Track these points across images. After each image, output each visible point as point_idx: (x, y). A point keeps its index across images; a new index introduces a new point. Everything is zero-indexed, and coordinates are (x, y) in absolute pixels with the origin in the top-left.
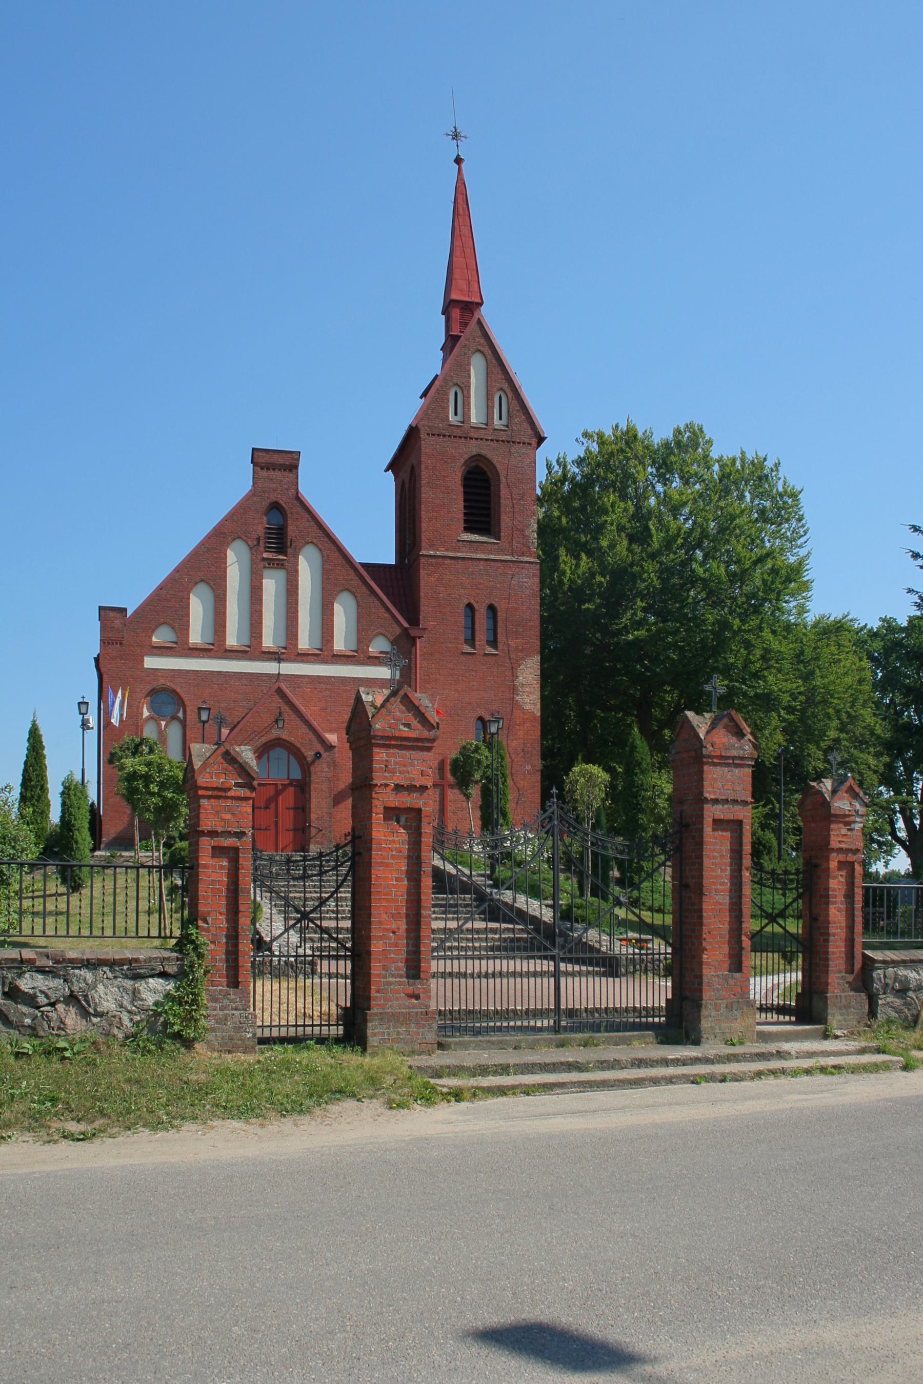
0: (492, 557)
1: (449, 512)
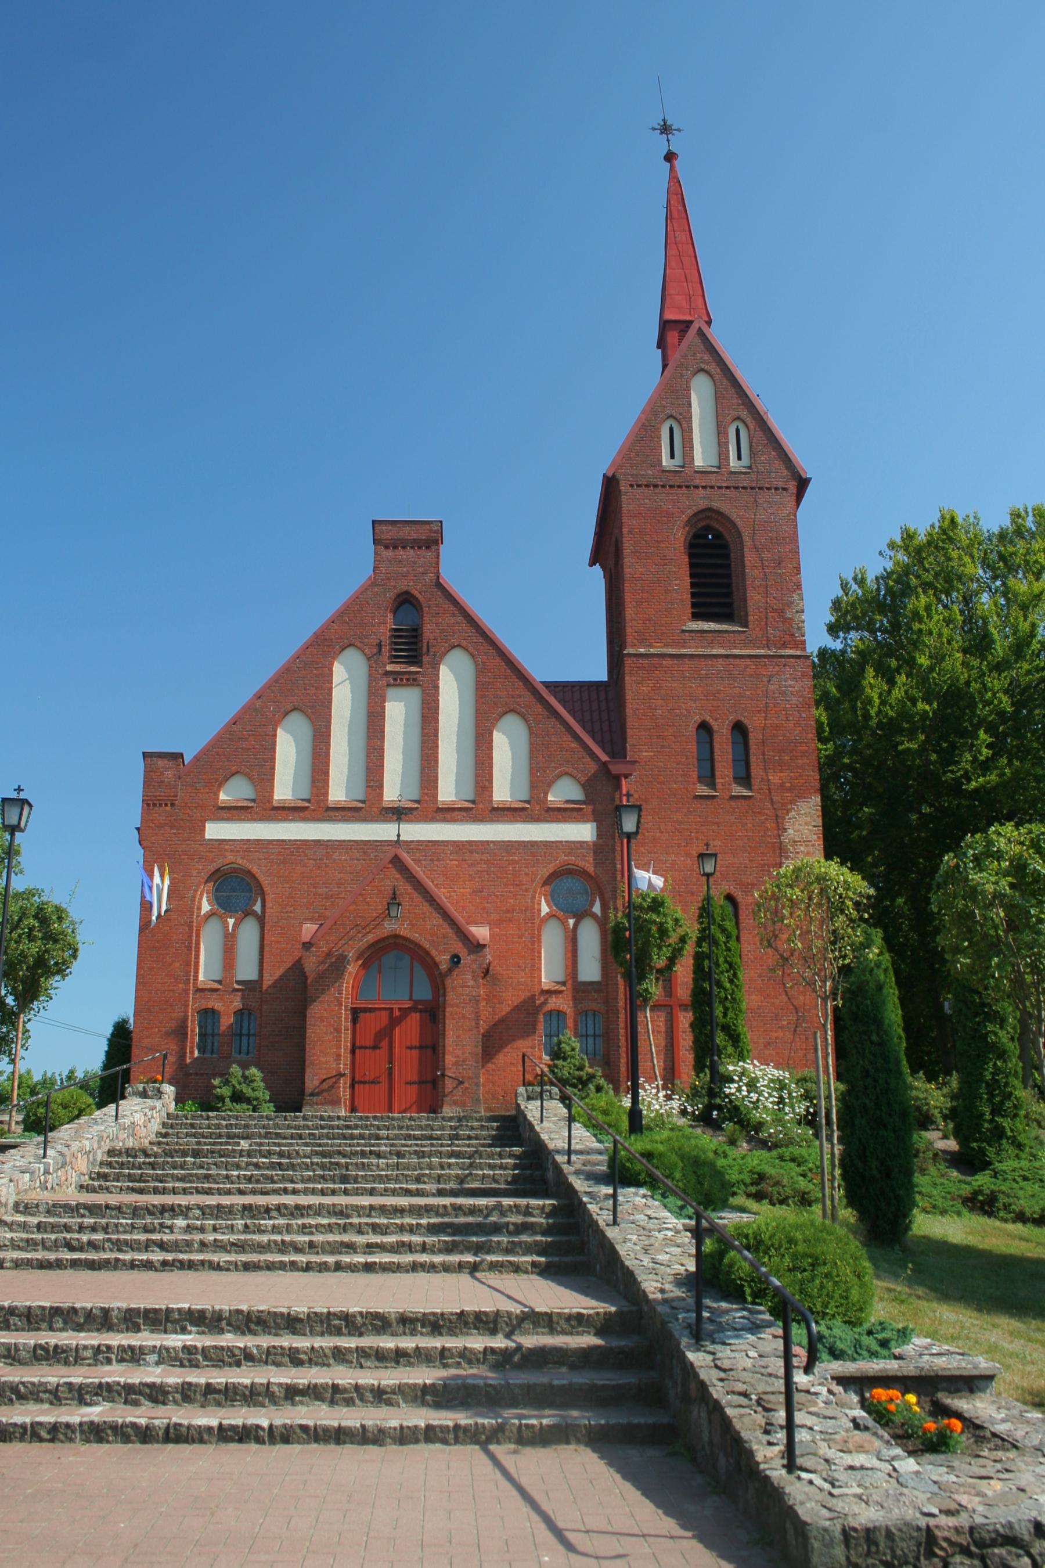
0: (737, 652)
1: (667, 591)
